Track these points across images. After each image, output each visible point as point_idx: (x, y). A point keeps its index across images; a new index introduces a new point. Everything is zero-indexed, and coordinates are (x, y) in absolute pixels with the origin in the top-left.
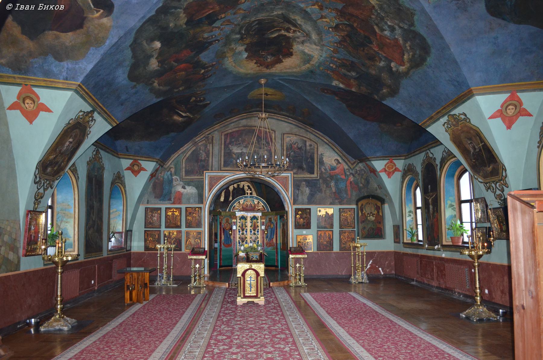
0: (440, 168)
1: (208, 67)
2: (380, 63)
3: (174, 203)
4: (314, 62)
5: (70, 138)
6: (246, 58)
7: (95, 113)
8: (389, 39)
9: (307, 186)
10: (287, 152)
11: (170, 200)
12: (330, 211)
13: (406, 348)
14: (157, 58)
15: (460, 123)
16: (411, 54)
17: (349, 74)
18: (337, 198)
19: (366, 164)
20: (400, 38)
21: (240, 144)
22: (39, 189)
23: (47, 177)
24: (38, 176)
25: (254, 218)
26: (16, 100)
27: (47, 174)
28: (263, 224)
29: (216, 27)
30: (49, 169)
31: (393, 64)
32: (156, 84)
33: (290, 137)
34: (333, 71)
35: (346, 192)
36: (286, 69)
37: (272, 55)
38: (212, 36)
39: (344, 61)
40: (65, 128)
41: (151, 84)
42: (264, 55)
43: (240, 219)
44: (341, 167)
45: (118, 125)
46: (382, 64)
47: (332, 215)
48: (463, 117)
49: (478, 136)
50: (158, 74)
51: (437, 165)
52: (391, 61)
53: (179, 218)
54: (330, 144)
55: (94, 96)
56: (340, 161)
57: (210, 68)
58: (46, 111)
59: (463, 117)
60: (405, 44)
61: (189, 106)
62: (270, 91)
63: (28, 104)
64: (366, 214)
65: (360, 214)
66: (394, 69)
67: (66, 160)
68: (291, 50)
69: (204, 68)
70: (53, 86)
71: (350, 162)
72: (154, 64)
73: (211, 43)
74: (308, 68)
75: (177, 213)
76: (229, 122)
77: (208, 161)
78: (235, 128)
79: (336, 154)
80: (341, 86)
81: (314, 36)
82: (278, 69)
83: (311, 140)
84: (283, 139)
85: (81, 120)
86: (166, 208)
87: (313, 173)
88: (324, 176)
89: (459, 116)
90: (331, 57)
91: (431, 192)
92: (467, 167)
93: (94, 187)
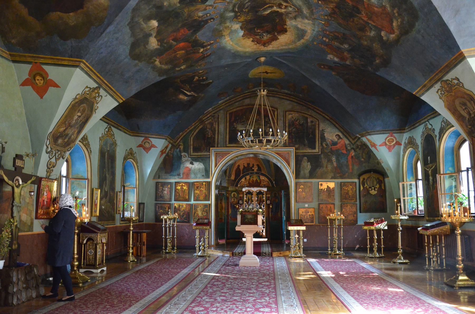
0: (439, 138)
1: (206, 46)
2: (370, 32)
3: (182, 178)
4: (308, 37)
5: (78, 112)
6: (243, 36)
7: (101, 89)
8: (376, 7)
9: (308, 161)
10: (289, 129)
11: (179, 175)
12: (332, 185)
13: (391, 298)
14: (155, 37)
15: (453, 88)
16: (399, 20)
17: (342, 46)
18: (339, 173)
19: (367, 139)
20: (387, 5)
21: (244, 121)
22: (51, 159)
23: (59, 148)
24: (49, 146)
25: (260, 193)
26: (27, 77)
27: (58, 145)
28: (268, 199)
29: (210, 6)
30: (60, 141)
31: (383, 33)
32: (157, 63)
33: (292, 114)
34: (327, 45)
35: (347, 166)
36: (282, 46)
37: (268, 32)
38: (206, 14)
39: (336, 34)
40: (73, 103)
41: (153, 63)
42: (260, 32)
43: (246, 194)
44: (342, 143)
45: (124, 101)
46: (372, 33)
47: (333, 188)
48: (456, 82)
49: (472, 100)
50: (159, 53)
51: (436, 136)
52: (380, 30)
53: (187, 192)
54: (331, 120)
55: (98, 73)
56: (342, 136)
57: (209, 47)
58: (54, 87)
59: (456, 82)
60: (393, 11)
61: (193, 85)
62: (269, 69)
63: (38, 80)
64: (368, 187)
65: (362, 188)
66: (385, 38)
67: (76, 133)
68: (285, 27)
69: (203, 47)
70: (60, 63)
71: (351, 137)
72: (153, 43)
73: (206, 22)
74: (303, 43)
75: (185, 188)
76: (233, 102)
77: (214, 138)
78: (239, 107)
79: (337, 130)
80: (336, 59)
81: (305, 11)
82: (273, 47)
83: (312, 117)
84: (285, 116)
85: (88, 96)
86: (175, 182)
87: (315, 148)
88: (326, 151)
89: (451, 82)
90: (323, 31)
91: (431, 163)
92: (466, 138)
93: (106, 161)
